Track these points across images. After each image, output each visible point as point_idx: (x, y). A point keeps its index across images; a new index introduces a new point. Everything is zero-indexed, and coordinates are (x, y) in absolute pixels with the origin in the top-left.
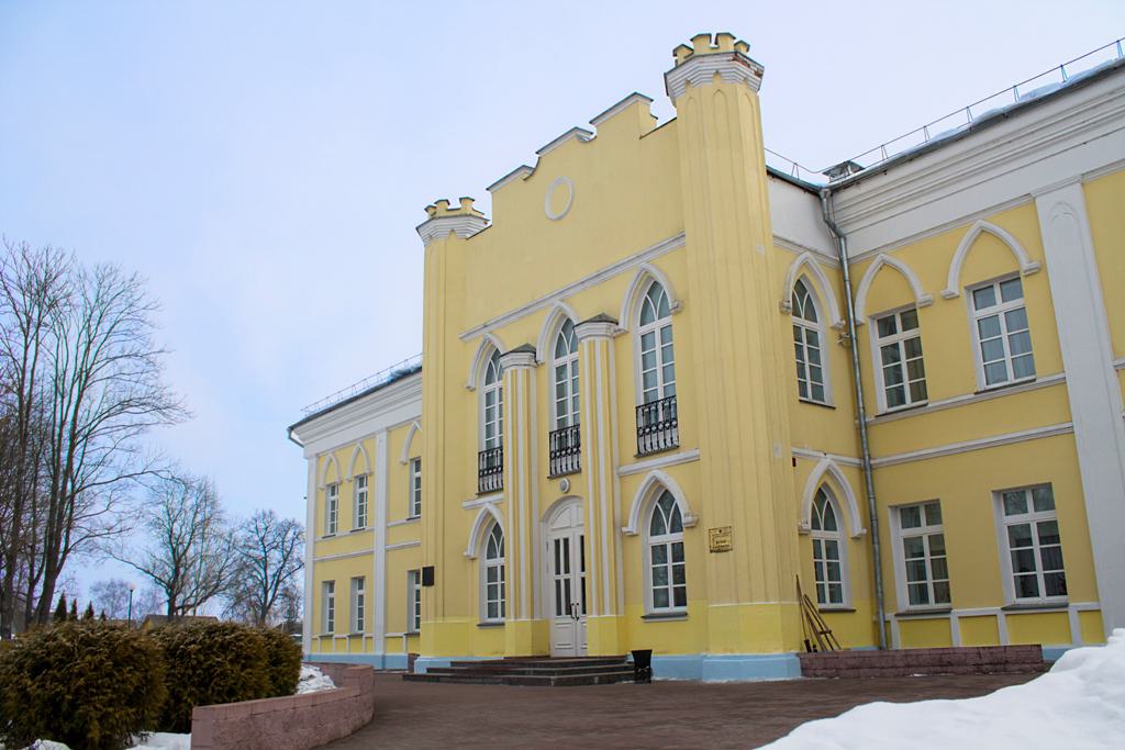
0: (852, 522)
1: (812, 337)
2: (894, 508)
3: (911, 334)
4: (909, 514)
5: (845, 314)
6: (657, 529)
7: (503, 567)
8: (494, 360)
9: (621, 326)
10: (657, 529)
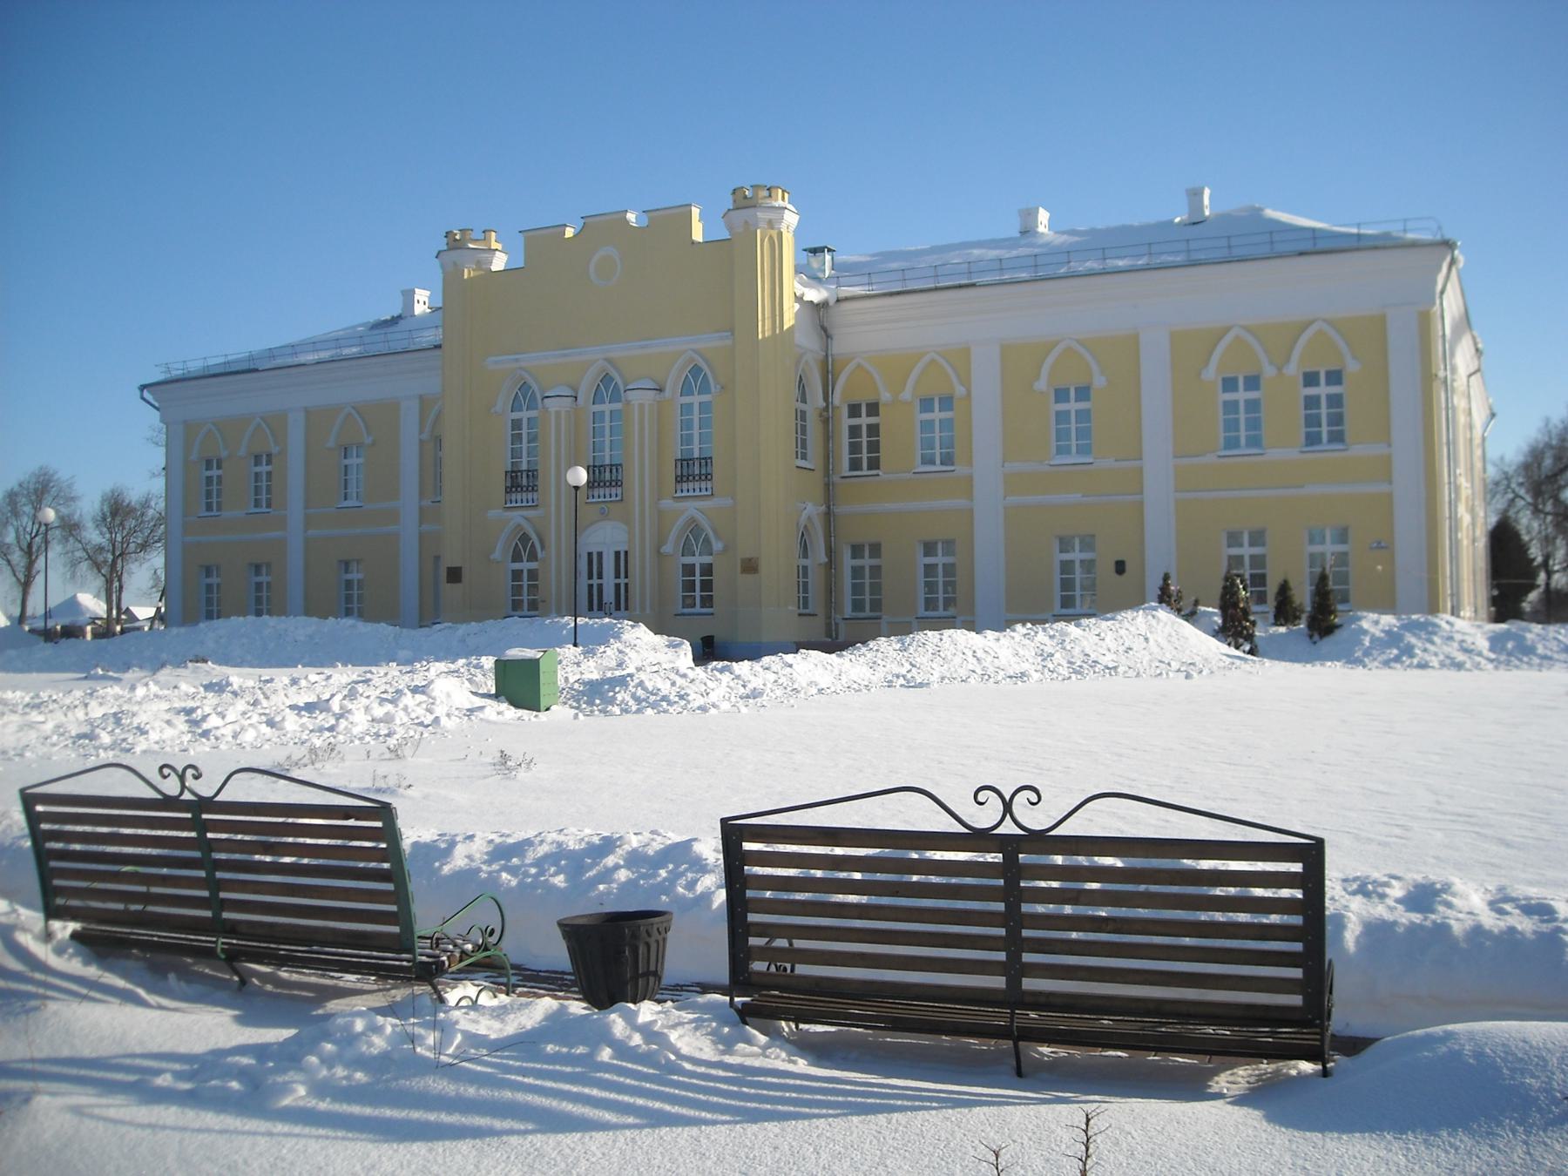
5: (826, 398)
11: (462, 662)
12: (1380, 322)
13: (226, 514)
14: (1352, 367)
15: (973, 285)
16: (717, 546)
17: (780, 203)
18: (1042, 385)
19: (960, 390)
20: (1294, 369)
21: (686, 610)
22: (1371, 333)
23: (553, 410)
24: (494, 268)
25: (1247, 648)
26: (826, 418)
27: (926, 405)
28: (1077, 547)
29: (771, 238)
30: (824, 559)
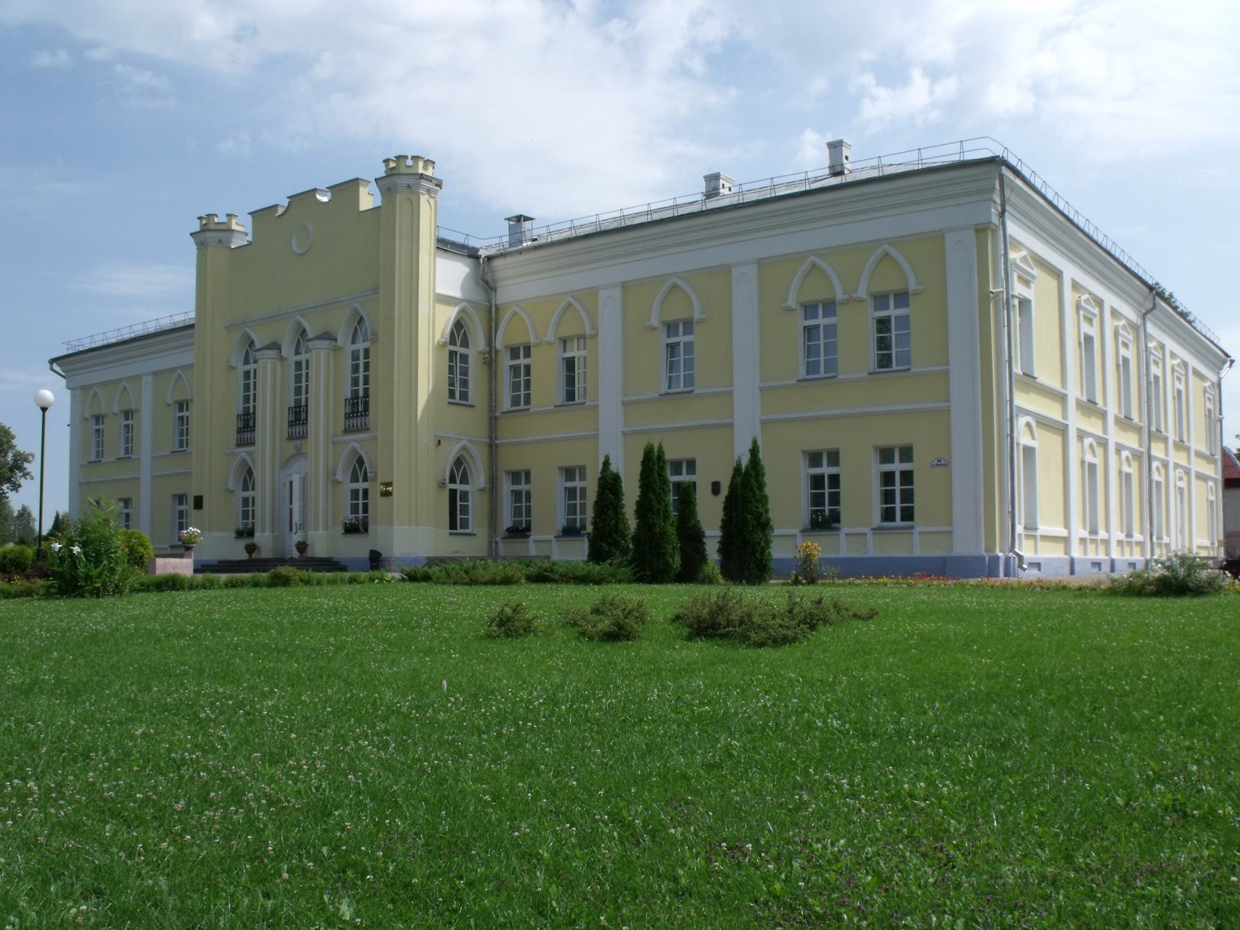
0: (479, 479)
1: (464, 358)
2: (508, 472)
4: (516, 476)
6: (355, 479)
7: (307, 361)
8: (249, 349)
9: (339, 343)
10: (355, 479)
28: (822, 371)
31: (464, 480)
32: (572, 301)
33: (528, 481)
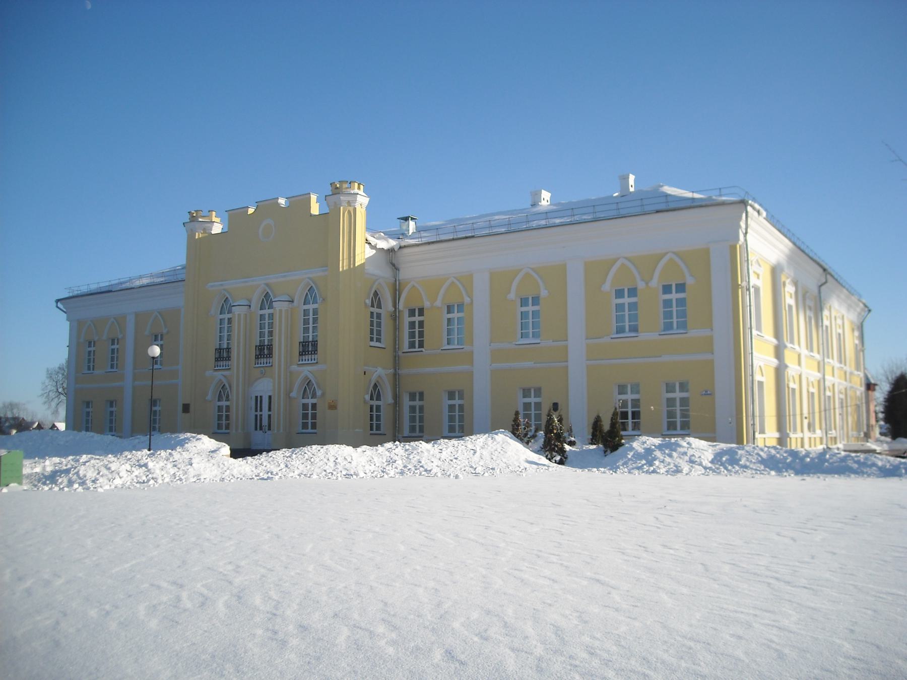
1: (379, 316)
3: (421, 318)
5: (395, 306)
11: (71, 458)
12: (706, 252)
13: (96, 372)
14: (690, 281)
15: (473, 237)
16: (319, 393)
17: (356, 191)
18: (512, 296)
19: (467, 300)
20: (655, 283)
21: (304, 431)
22: (700, 260)
23: (236, 313)
24: (213, 232)
25: (558, 458)
26: (395, 316)
27: (450, 309)
28: (629, 392)
29: (349, 212)
30: (390, 400)
31: (378, 398)
32: (455, 280)
33: (421, 399)
